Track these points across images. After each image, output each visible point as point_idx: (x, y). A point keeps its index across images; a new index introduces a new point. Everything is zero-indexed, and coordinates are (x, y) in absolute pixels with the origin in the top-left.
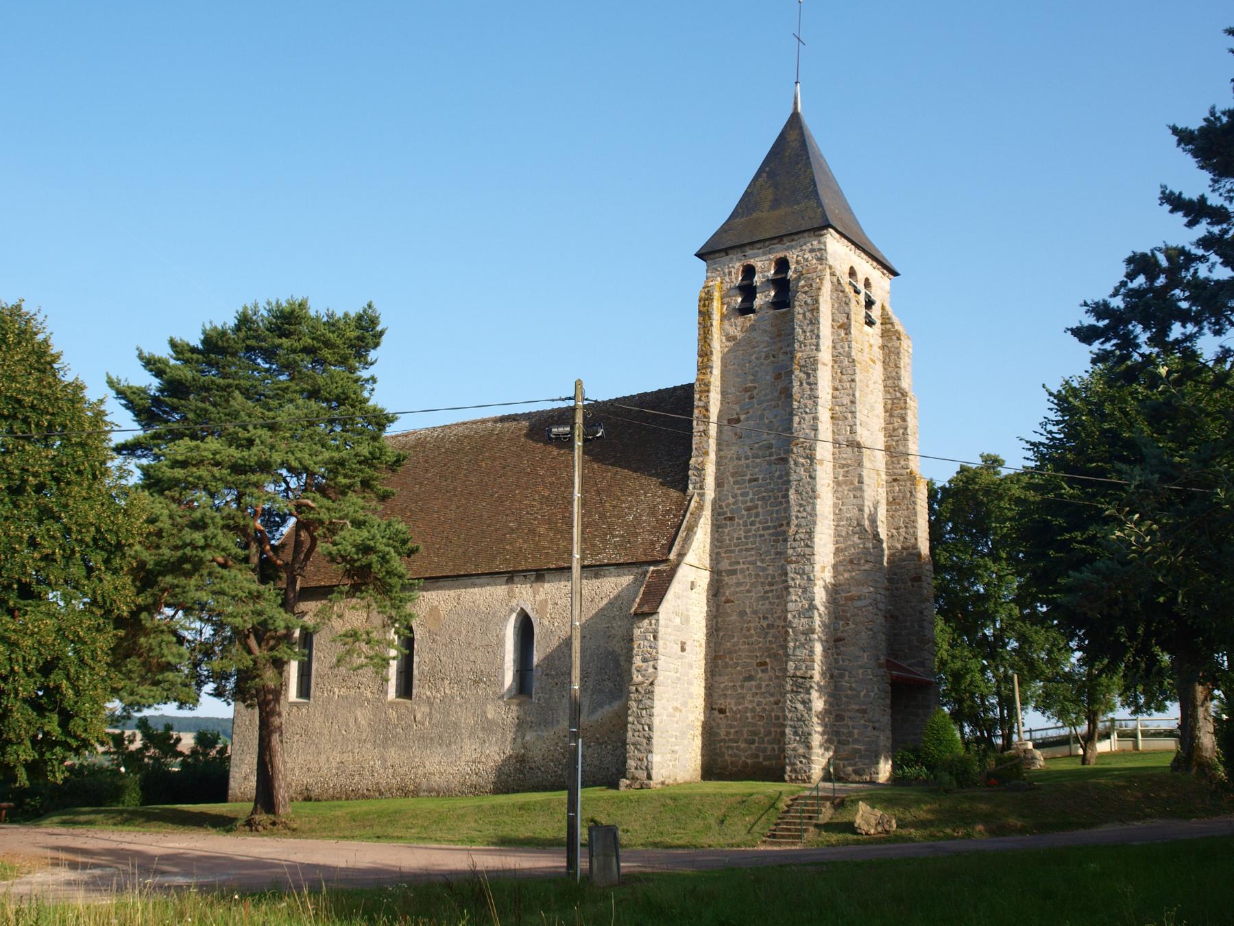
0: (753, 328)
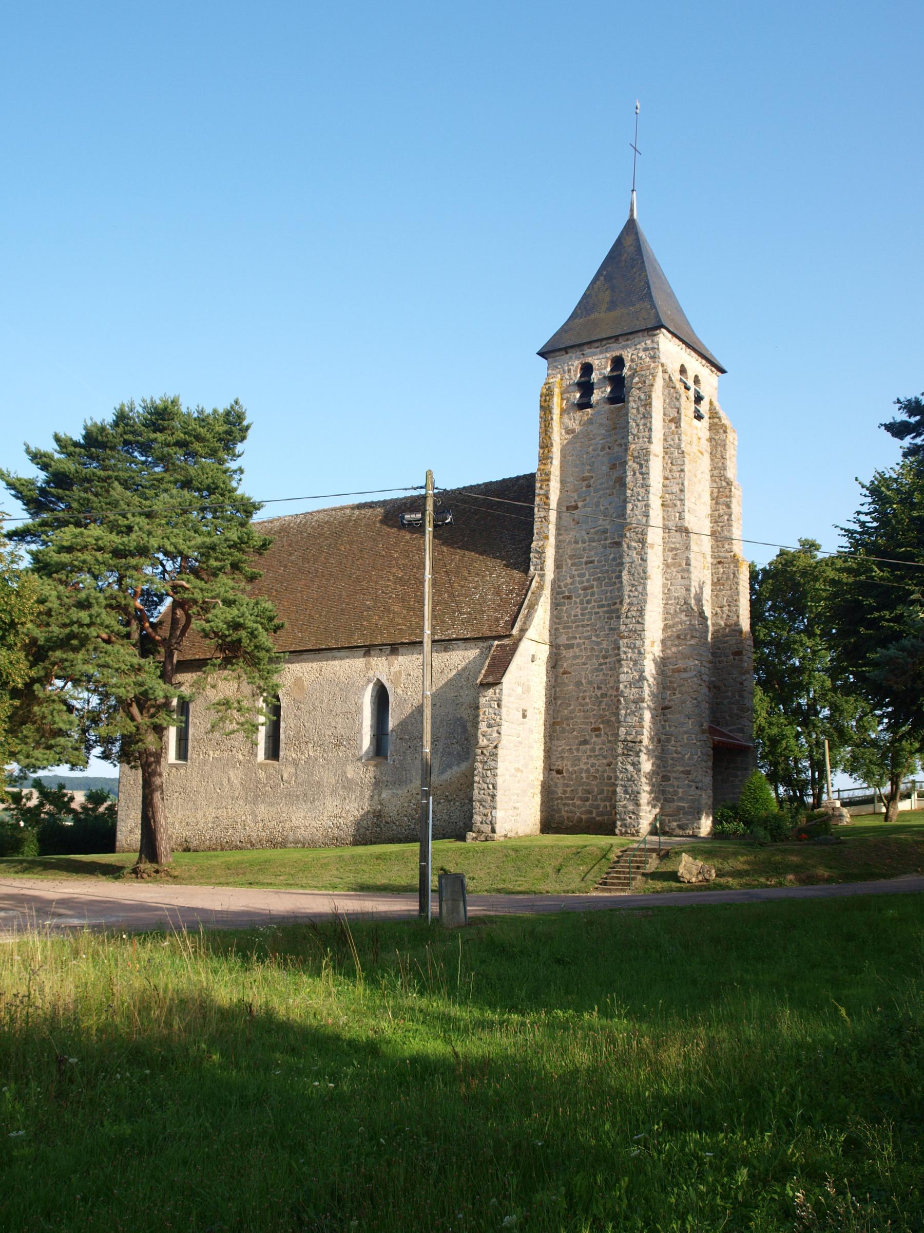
0: (590, 422)
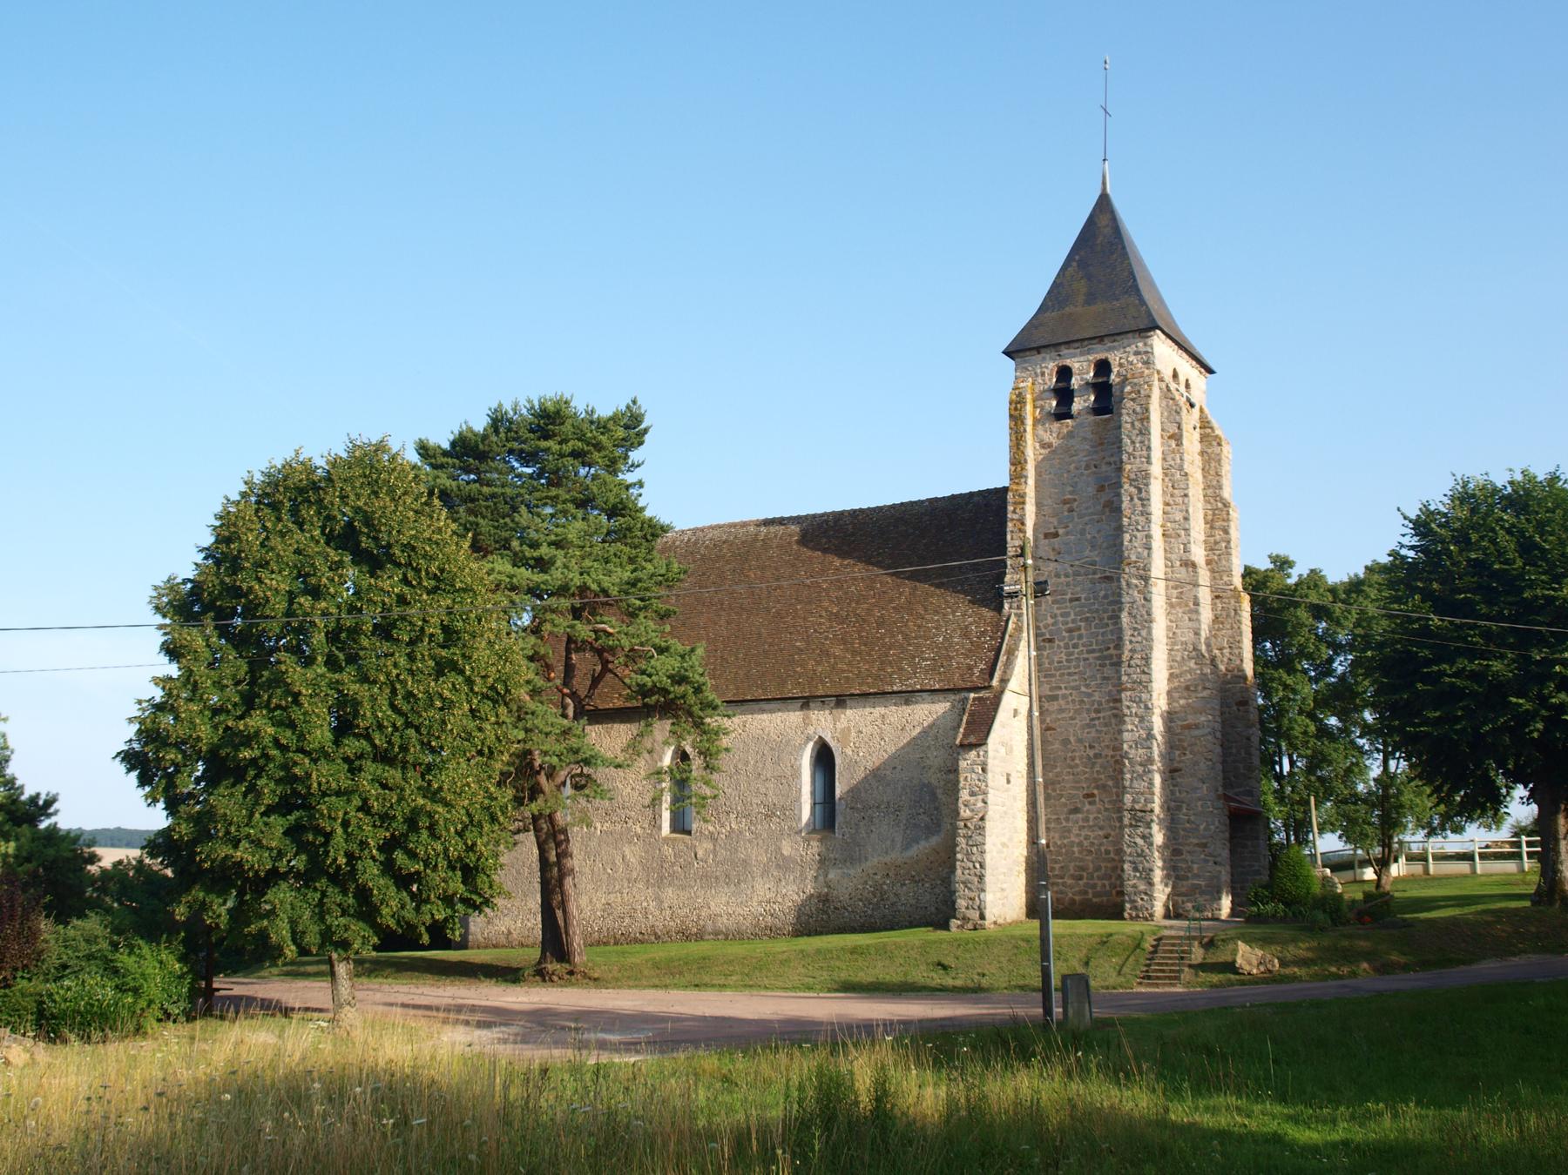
0: (1070, 435)
